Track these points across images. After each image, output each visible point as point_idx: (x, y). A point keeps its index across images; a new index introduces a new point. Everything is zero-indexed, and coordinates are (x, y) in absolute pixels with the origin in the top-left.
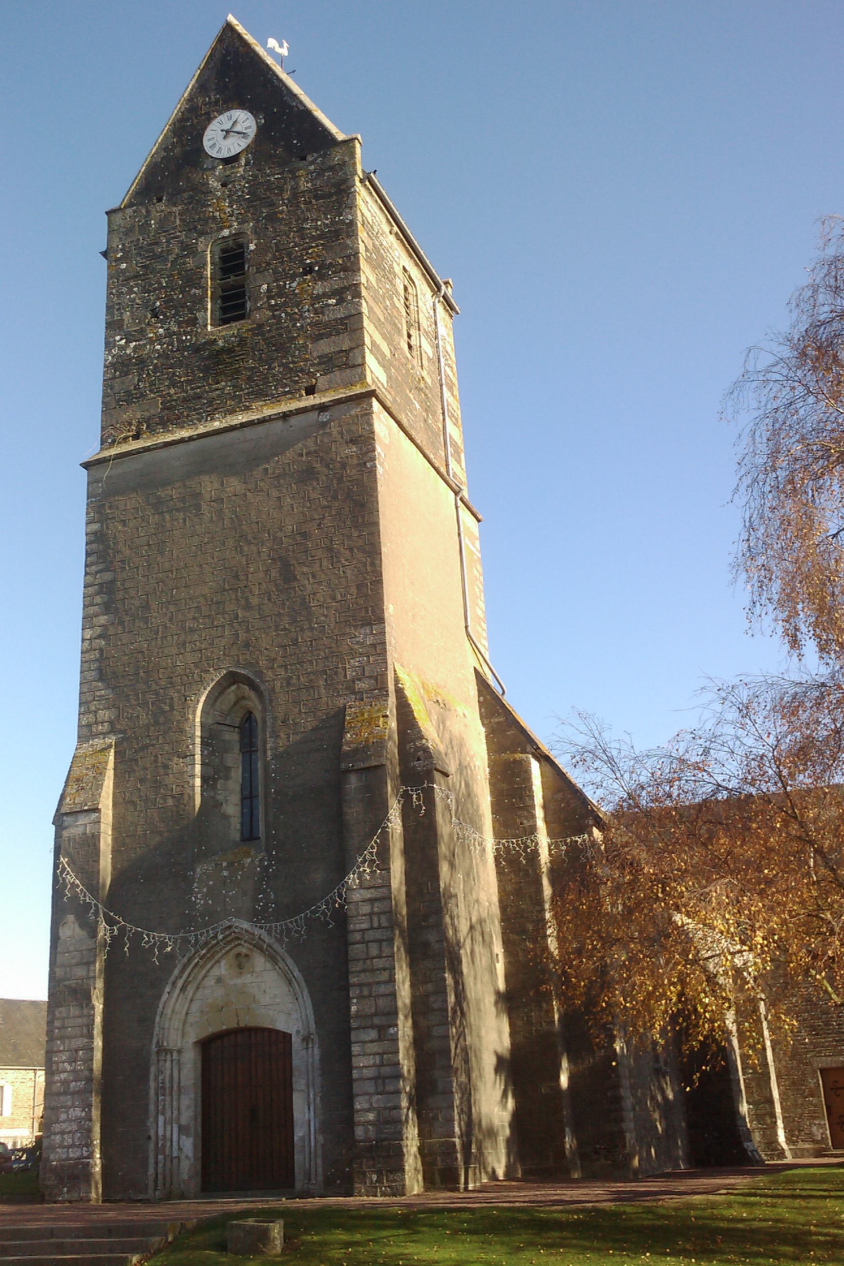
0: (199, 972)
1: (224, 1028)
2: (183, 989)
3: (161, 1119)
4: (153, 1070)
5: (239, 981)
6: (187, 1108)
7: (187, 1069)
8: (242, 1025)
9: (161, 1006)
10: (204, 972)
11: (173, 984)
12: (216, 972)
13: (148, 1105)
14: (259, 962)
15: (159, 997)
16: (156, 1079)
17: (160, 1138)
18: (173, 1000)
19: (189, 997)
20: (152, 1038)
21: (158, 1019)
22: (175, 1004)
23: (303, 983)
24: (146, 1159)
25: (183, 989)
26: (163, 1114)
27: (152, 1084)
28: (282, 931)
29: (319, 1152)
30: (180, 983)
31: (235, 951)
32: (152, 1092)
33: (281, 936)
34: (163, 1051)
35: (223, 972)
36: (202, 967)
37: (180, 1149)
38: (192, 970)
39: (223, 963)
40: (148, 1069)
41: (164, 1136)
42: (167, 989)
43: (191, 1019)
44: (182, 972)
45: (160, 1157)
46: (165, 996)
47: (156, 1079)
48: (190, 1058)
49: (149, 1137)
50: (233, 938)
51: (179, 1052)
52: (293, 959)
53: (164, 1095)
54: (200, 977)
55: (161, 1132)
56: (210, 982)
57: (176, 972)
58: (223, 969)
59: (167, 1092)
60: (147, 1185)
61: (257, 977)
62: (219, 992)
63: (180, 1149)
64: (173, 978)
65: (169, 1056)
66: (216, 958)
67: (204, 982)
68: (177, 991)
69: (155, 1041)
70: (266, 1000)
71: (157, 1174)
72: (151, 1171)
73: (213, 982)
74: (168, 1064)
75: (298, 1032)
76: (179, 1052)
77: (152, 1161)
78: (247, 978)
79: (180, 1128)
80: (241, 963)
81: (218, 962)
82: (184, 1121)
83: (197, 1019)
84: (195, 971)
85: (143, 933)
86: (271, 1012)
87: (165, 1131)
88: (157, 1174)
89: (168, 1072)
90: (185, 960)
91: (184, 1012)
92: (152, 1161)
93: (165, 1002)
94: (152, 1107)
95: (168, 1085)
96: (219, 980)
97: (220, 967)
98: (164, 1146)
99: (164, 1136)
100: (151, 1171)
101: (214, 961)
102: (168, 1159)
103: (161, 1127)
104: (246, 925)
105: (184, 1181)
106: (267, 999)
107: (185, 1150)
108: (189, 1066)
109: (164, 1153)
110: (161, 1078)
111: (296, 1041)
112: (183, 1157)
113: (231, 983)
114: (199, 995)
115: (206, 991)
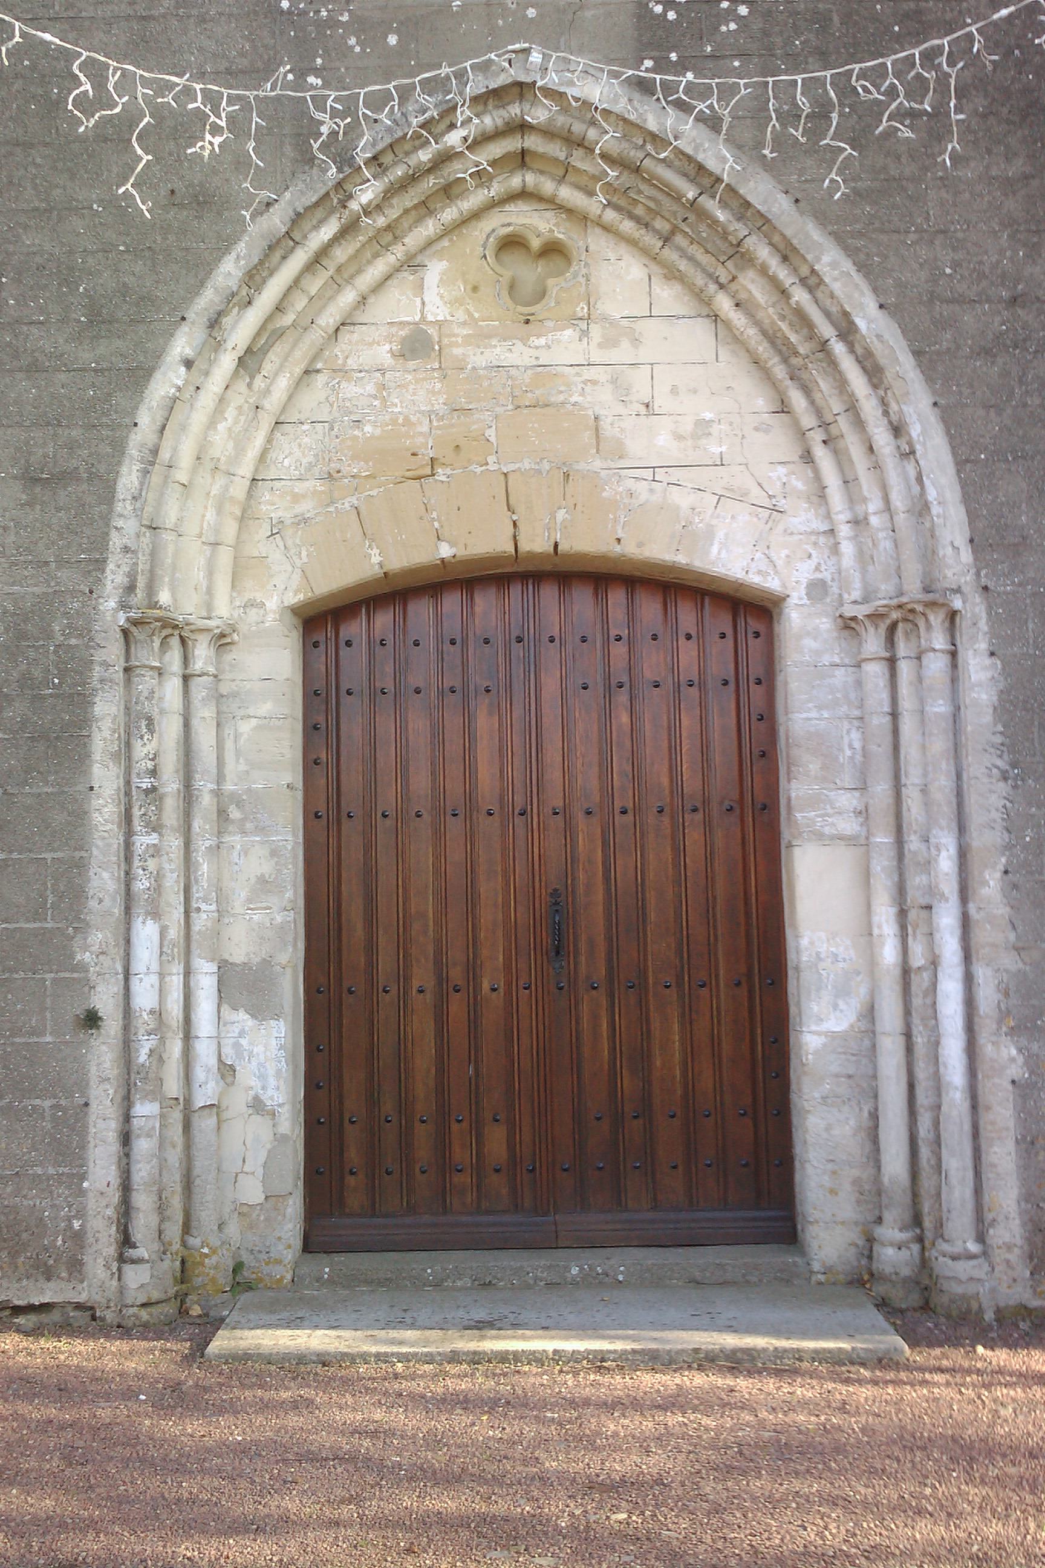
0: (318, 302)
1: (445, 551)
2: (249, 360)
3: (146, 932)
4: (106, 709)
5: (516, 355)
6: (252, 891)
7: (250, 727)
8: (536, 543)
9: (147, 419)
10: (348, 297)
11: (214, 324)
12: (398, 306)
13: (80, 866)
14: (620, 276)
15: (139, 375)
16: (125, 754)
17: (144, 1020)
18: (207, 400)
19: (273, 402)
20: (100, 564)
21: (128, 478)
22: (212, 424)
23: (903, 365)
24: (73, 1121)
25: (249, 360)
26: (155, 914)
27: (105, 777)
28: (821, 113)
29: (1002, 1114)
30: (242, 330)
31: (497, 223)
32: (104, 813)
33: (815, 133)
34: (152, 626)
35: (437, 309)
36: (341, 278)
37: (227, 1071)
38: (296, 283)
39: (435, 270)
40: (78, 703)
41: (159, 1014)
42: (182, 344)
43: (272, 505)
44: (255, 278)
45: (145, 1109)
46: (168, 379)
47: (125, 754)
48: (270, 670)
49: (92, 1020)
50: (529, 140)
51: (222, 641)
52: (850, 251)
53: (156, 828)
54: (329, 319)
55: (144, 997)
56: (372, 348)
57: (229, 270)
58: (435, 296)
59: (171, 815)
60: (78, 1238)
61: (609, 343)
62: (418, 397)
63: (227, 1071)
64: (207, 299)
65: (174, 657)
66: (414, 239)
67: (339, 350)
68: (227, 362)
69: (114, 576)
70: (655, 442)
71: (126, 1187)
72: (102, 1171)
73: (383, 354)
74: (172, 687)
75: (817, 589)
76: (222, 641)
77: (103, 1127)
78: (562, 346)
79: (225, 972)
80: (533, 266)
81: (412, 264)
82: (241, 947)
83: (306, 507)
84: (314, 284)
85: (70, 57)
86: (682, 499)
87: (162, 992)
88: (126, 1187)
89: (171, 728)
90: (276, 220)
91: (246, 469)
92: (103, 1127)
93: (172, 404)
94: (103, 881)
95: (171, 784)
96: (417, 344)
97: (420, 287)
98: (158, 1055)
99: (159, 1014)
100: (102, 1171)
101: (398, 252)
102: (176, 1116)
103: (146, 971)
104: (599, 90)
105: (243, 1211)
106: (663, 439)
107: (248, 1077)
108: (266, 708)
109: (156, 1092)
110: (141, 750)
111: (806, 636)
112: (238, 1102)
113: (479, 358)
114: (315, 398)
115: (350, 390)
